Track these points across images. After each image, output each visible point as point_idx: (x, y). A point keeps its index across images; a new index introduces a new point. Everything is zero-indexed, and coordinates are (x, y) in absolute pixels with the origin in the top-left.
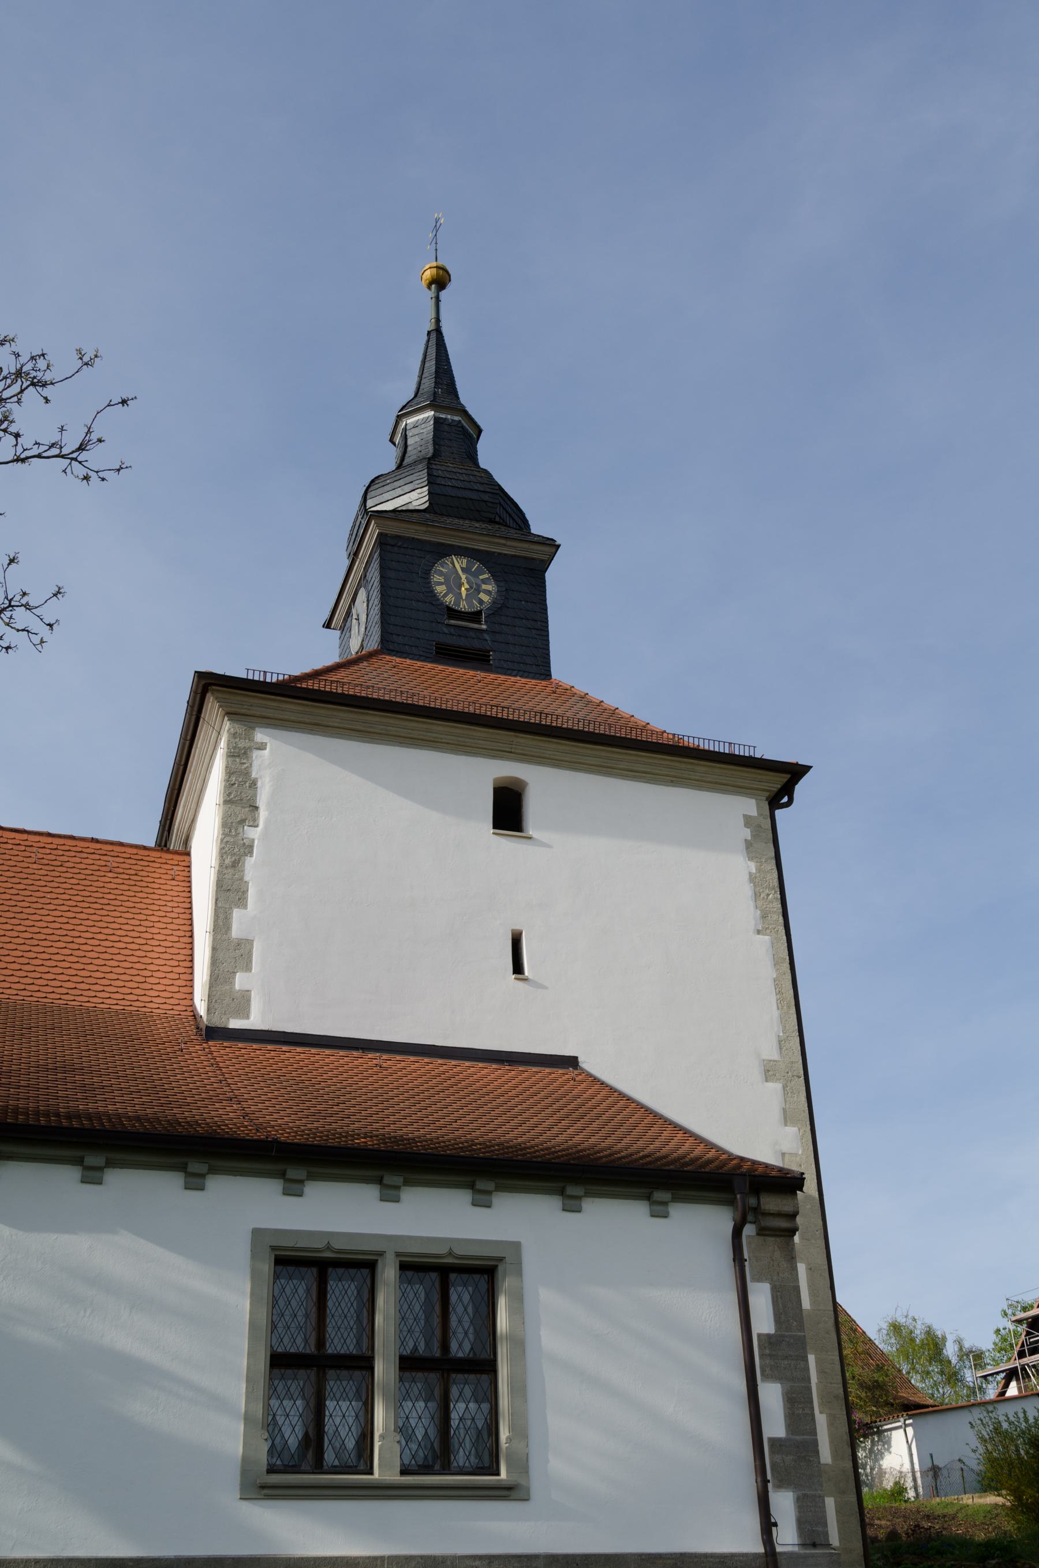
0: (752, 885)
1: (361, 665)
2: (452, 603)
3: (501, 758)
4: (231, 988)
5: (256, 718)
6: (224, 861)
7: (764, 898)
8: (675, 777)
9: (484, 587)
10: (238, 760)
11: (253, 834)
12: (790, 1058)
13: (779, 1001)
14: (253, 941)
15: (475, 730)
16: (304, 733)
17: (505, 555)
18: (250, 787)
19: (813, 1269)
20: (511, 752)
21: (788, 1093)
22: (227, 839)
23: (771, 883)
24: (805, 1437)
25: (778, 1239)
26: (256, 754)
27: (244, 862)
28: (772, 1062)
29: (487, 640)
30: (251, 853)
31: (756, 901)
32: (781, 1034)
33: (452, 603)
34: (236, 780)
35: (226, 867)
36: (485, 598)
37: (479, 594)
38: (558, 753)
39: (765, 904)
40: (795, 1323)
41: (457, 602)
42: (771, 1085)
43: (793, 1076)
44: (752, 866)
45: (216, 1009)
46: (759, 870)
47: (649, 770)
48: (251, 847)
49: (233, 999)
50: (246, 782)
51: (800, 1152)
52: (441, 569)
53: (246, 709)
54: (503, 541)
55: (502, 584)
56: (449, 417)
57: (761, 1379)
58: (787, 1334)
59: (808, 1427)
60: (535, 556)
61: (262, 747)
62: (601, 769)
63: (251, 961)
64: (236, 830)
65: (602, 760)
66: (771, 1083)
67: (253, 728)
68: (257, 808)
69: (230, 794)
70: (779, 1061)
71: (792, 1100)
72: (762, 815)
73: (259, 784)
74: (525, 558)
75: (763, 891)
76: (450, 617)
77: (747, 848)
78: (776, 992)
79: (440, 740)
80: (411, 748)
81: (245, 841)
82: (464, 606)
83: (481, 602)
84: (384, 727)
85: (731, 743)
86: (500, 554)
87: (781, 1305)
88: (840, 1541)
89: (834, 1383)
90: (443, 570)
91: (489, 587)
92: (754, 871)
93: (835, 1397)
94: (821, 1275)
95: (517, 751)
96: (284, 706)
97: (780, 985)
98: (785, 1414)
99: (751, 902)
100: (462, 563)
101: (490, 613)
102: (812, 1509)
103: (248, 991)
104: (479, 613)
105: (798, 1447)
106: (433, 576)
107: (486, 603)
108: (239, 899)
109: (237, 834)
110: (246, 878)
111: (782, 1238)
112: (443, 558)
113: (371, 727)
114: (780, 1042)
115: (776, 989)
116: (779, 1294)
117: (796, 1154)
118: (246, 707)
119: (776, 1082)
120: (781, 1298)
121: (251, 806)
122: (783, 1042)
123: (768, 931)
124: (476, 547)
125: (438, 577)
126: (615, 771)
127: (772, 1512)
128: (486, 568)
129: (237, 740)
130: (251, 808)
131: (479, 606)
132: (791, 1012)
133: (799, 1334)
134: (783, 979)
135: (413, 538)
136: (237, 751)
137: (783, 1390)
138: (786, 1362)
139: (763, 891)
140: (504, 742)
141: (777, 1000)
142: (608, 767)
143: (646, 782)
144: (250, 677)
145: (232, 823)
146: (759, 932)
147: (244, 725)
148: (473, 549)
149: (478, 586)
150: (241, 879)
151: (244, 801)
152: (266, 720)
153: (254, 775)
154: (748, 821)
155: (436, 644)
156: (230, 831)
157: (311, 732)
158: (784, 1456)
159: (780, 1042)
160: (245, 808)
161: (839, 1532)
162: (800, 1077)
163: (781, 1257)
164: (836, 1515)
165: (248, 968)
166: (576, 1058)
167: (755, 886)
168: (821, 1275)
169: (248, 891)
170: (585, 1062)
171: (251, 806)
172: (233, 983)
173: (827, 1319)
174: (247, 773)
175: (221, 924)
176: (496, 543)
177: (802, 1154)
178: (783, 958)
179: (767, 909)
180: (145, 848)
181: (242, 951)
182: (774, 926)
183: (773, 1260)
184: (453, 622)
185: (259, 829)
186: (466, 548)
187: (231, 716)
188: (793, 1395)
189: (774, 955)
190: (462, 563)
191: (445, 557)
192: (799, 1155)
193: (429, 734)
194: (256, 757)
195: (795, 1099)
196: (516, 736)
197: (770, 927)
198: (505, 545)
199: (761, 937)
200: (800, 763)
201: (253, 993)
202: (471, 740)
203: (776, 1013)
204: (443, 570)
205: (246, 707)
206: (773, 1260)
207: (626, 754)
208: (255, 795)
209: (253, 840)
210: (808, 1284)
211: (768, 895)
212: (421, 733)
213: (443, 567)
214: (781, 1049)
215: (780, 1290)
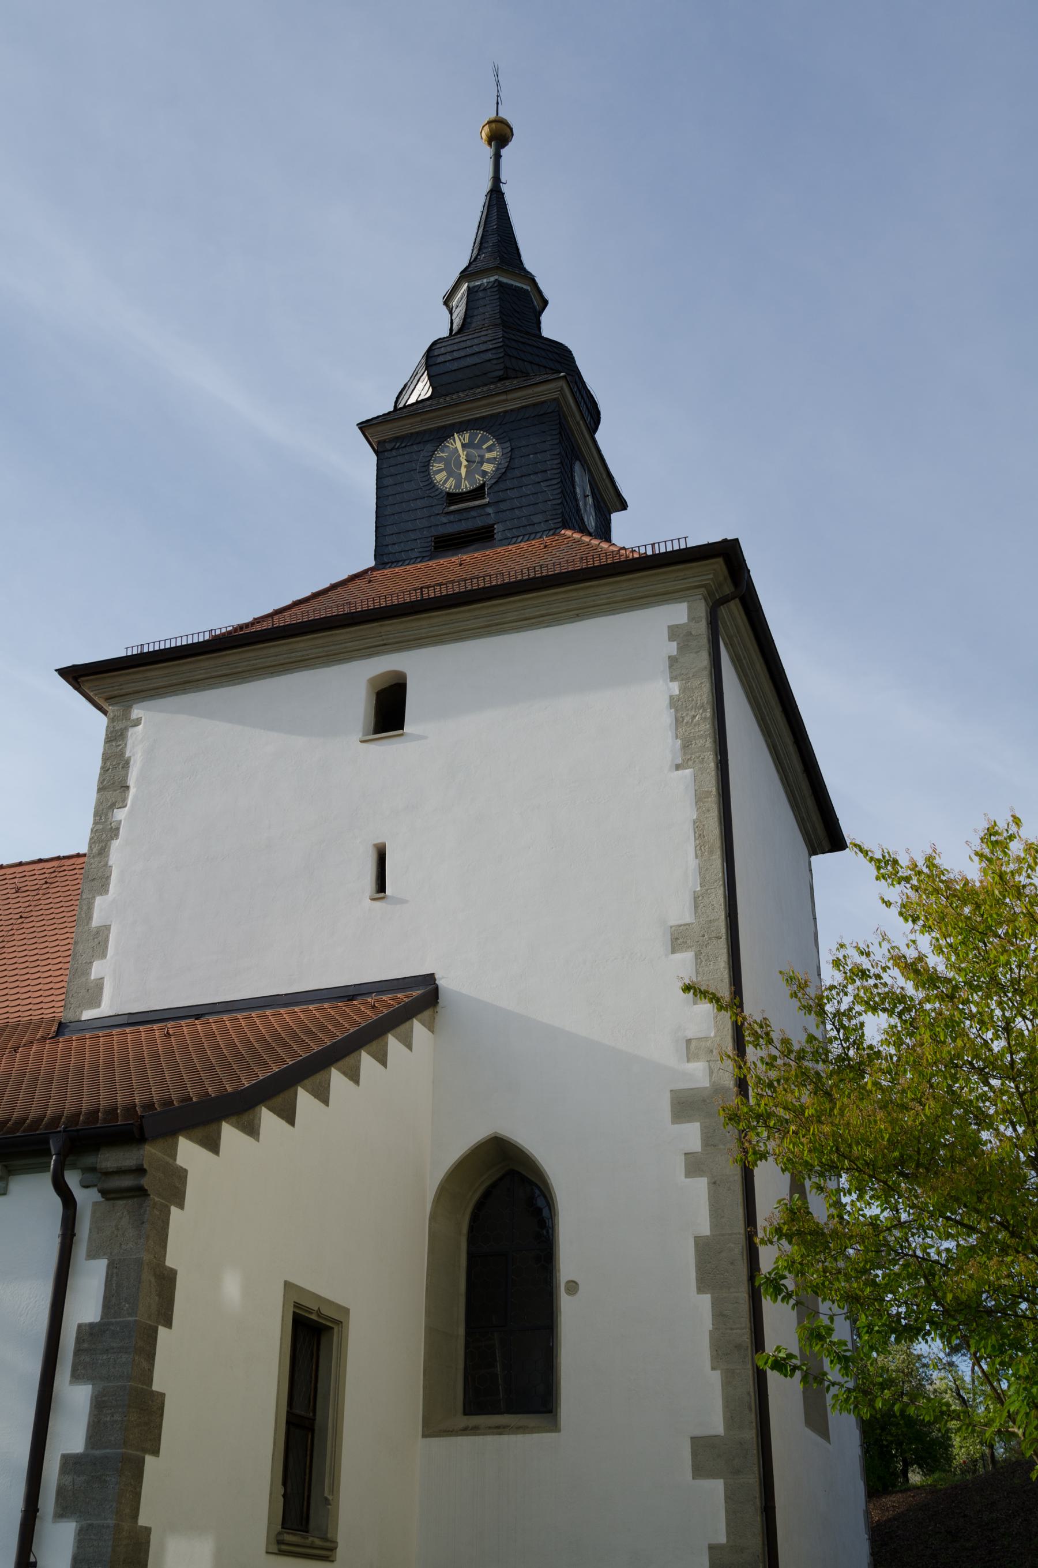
0: (673, 710)
1: (339, 589)
2: (468, 486)
3: (377, 654)
4: (87, 979)
5: (132, 695)
6: (92, 851)
7: (687, 722)
8: (581, 609)
9: (488, 455)
10: (114, 744)
11: (120, 815)
12: (708, 917)
13: (698, 847)
14: (110, 925)
15: (336, 634)
16: (177, 695)
17: (512, 410)
18: (123, 767)
19: (718, 1182)
20: (385, 645)
21: (702, 961)
22: (100, 827)
23: (699, 701)
24: (108, 1451)
25: (130, 1202)
26: (131, 731)
27: (110, 847)
28: (681, 928)
29: (490, 514)
30: (117, 836)
31: (676, 729)
32: (699, 889)
33: (468, 486)
34: (110, 765)
35: (93, 857)
36: (488, 467)
37: (482, 465)
38: (435, 628)
39: (688, 729)
40: (127, 1305)
41: (458, 485)
42: (679, 956)
43: (710, 939)
44: (675, 688)
45: (71, 1004)
46: (683, 690)
47: (545, 612)
48: (118, 829)
49: (88, 990)
50: (119, 764)
51: (712, 1035)
52: (442, 454)
53: (118, 689)
54: (503, 397)
55: (508, 444)
56: (485, 281)
57: (70, 1381)
58: (114, 1320)
59: (113, 1439)
60: (543, 398)
61: (137, 722)
62: (489, 629)
63: (107, 947)
64: (106, 815)
65: (485, 619)
66: (679, 954)
67: (130, 707)
68: (128, 787)
69: (104, 780)
70: (692, 924)
71: (706, 969)
72: (693, 619)
73: (132, 762)
74: (534, 405)
75: (687, 715)
76: (451, 504)
77: (671, 666)
78: (695, 836)
79: (307, 657)
80: (282, 675)
81: (112, 825)
82: (466, 486)
83: (484, 473)
84: (248, 663)
85: (654, 544)
86: (506, 412)
87: (114, 1285)
88: (727, 1537)
89: (737, 1329)
90: (443, 455)
91: (493, 454)
92: (677, 692)
93: (736, 1347)
94: (729, 1189)
95: (390, 641)
96: (148, 674)
97: (702, 827)
98: (89, 1423)
99: (670, 733)
100: (464, 439)
101: (492, 482)
102: (95, 1543)
103: (102, 978)
104: (483, 486)
105: (95, 1464)
106: (433, 466)
107: (490, 473)
108: (103, 886)
109: (107, 819)
110: (110, 863)
111: (135, 1200)
112: (443, 442)
113: (236, 667)
114: (696, 899)
115: (695, 833)
116: (115, 1271)
117: (706, 1038)
118: (116, 688)
119: (686, 951)
120: (117, 1275)
121: (122, 787)
122: (700, 899)
123: (690, 763)
124: (478, 416)
125: (438, 465)
126: (505, 625)
127: (33, 1549)
128: (490, 434)
129: (115, 724)
130: (123, 788)
131: (481, 479)
132: (714, 857)
133: (130, 1319)
134: (707, 818)
135: (412, 434)
136: (113, 734)
137: (93, 1393)
138: (105, 1357)
139: (687, 715)
140: (372, 636)
141: (696, 847)
142: (497, 625)
143: (547, 627)
144: (130, 653)
145: (103, 810)
146: (678, 767)
147: (123, 706)
148: (476, 419)
149: (482, 457)
150: (106, 865)
151: (117, 783)
152: (141, 694)
153: (127, 755)
154: (674, 632)
155: (435, 539)
156: (101, 819)
157: (185, 691)
158: (75, 1477)
159: (696, 899)
160: (115, 791)
161: (728, 1525)
162: (721, 938)
163: (129, 1223)
164: (726, 1502)
165: (104, 955)
166: (432, 975)
167: (677, 711)
168: (729, 1189)
169: (111, 875)
170: (443, 978)
171: (122, 787)
172: (89, 974)
173: (732, 1245)
174: (122, 754)
175: (84, 916)
176: (498, 402)
177: (715, 1036)
178: (708, 792)
179: (692, 735)
180: (78, 855)
181: (100, 938)
182: (697, 754)
183: (118, 1229)
184: (453, 508)
185: (126, 809)
186: (469, 421)
187: (109, 701)
188: (104, 1399)
189: (696, 791)
190: (464, 439)
191: (446, 440)
192: (711, 1038)
193: (293, 655)
194: (132, 734)
195: (711, 967)
196: (381, 626)
197: (693, 756)
198: (507, 400)
199: (680, 772)
200: (729, 539)
201: (105, 980)
202: (337, 647)
203: (692, 862)
204: (443, 455)
205: (116, 688)
206: (118, 1229)
207: (509, 602)
208: (127, 775)
209: (121, 821)
210: (710, 1202)
211: (694, 717)
212: (285, 656)
213: (443, 452)
214: (696, 907)
215: (118, 1266)
